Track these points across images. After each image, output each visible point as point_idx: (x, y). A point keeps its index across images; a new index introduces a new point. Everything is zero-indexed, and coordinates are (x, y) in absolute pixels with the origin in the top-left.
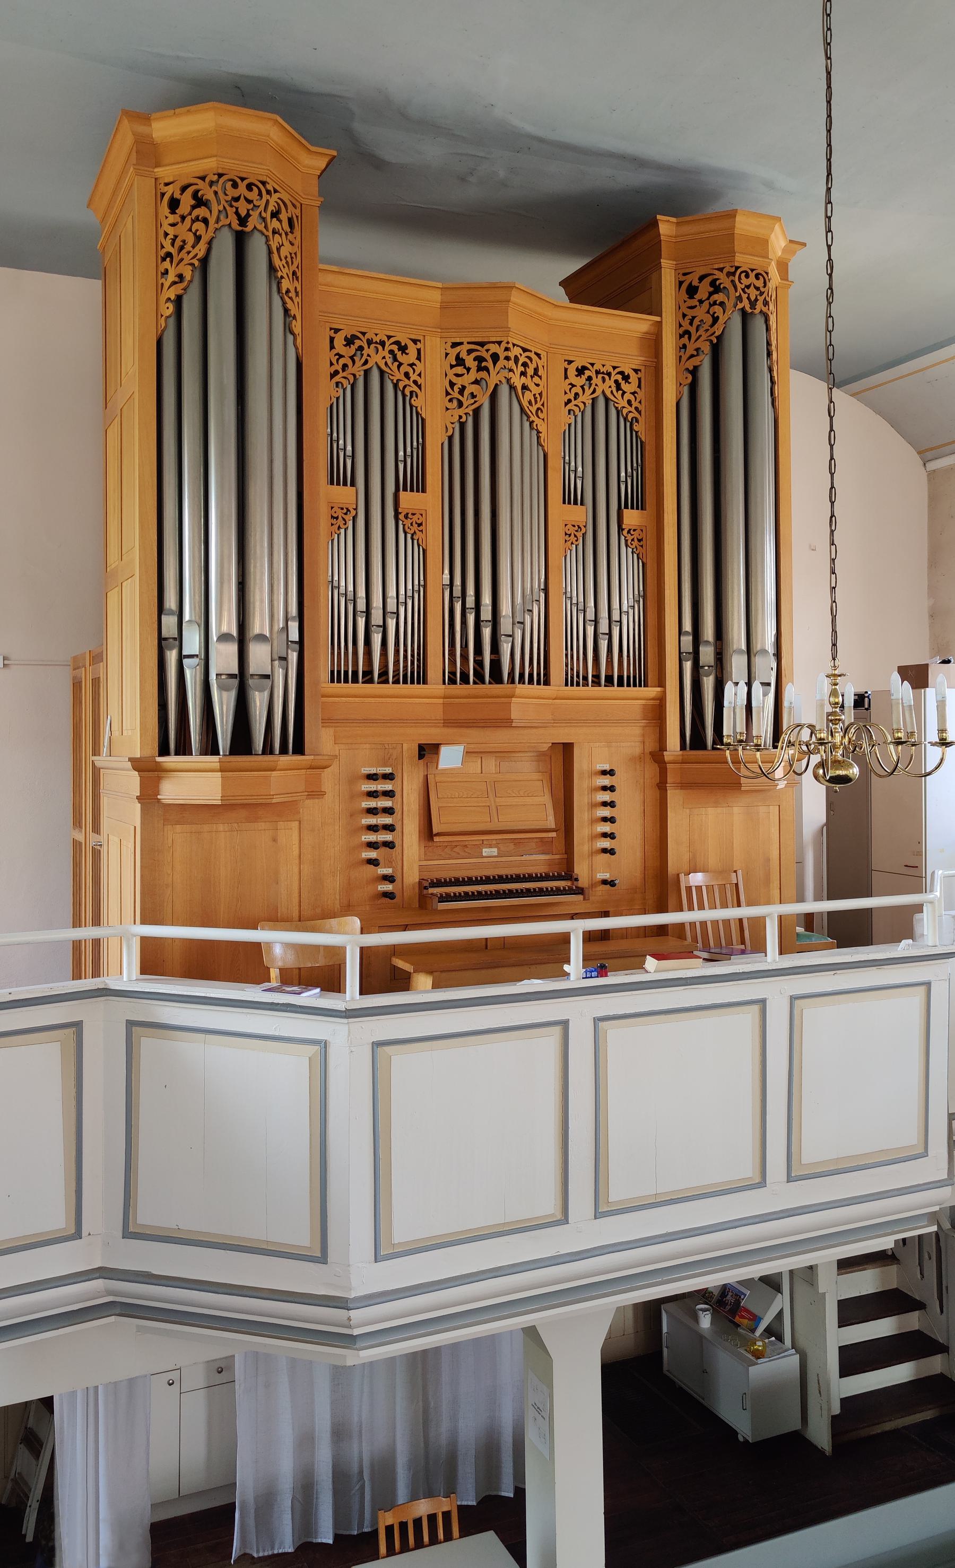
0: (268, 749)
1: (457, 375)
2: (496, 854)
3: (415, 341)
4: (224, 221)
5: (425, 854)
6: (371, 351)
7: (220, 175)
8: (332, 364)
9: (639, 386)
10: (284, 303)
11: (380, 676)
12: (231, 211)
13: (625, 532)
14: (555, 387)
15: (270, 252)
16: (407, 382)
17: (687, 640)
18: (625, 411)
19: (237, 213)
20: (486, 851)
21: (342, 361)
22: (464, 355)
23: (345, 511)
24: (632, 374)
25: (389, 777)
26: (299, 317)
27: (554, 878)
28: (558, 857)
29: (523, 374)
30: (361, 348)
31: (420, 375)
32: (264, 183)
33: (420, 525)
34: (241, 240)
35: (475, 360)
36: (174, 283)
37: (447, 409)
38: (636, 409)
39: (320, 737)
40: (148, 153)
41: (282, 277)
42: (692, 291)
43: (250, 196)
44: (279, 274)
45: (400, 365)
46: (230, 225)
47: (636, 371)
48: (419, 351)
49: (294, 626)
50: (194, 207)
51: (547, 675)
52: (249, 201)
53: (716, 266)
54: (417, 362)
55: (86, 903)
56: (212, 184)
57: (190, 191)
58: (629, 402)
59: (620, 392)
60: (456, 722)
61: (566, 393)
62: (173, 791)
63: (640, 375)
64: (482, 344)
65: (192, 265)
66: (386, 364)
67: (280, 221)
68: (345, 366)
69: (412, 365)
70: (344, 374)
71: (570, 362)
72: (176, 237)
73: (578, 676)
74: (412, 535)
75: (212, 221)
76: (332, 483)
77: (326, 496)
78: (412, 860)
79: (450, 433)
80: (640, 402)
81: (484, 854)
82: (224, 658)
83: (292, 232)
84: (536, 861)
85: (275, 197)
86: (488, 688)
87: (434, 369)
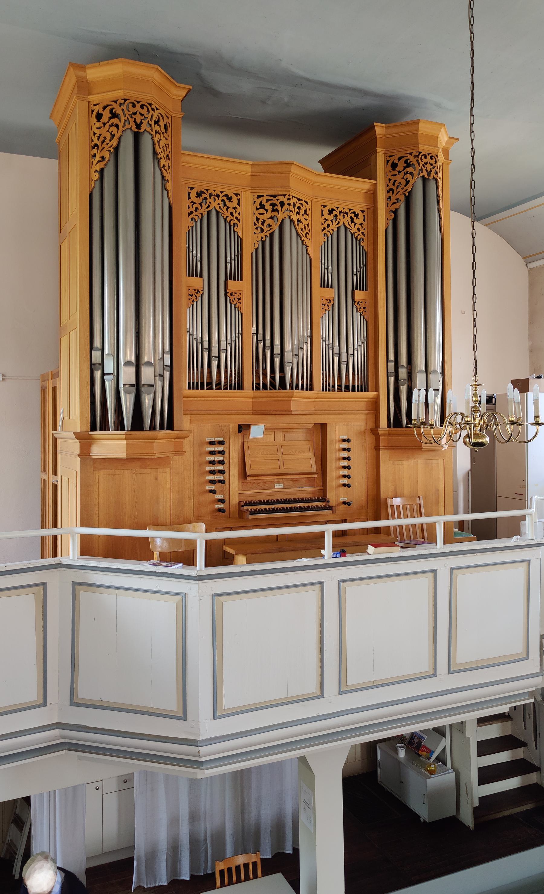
0: (153, 427)
1: (260, 214)
2: (282, 487)
3: (236, 195)
4: (127, 126)
5: (242, 487)
6: (212, 200)
7: (125, 100)
8: (189, 208)
9: (364, 220)
10: (162, 173)
11: (216, 385)
12: (132, 120)
13: (356, 303)
14: (316, 221)
15: (154, 144)
16: (232, 218)
17: (392, 365)
18: (356, 235)
19: (135, 121)
20: (277, 485)
21: (195, 206)
22: (264, 202)
23: (197, 291)
24: (360, 213)
25: (221, 443)
26: (170, 181)
27: (315, 501)
28: (318, 488)
29: (298, 213)
30: (205, 199)
31: (239, 214)
32: (150, 104)
33: (239, 299)
34: (137, 137)
35: (270, 205)
36: (99, 161)
37: (255, 233)
38: (363, 233)
39: (182, 420)
40: (84, 87)
41: (161, 158)
42: (394, 166)
43: (142, 111)
44: (159, 156)
45: (228, 208)
46: (131, 128)
47: (362, 211)
48: (239, 200)
49: (167, 357)
50: (110, 118)
51: (311, 384)
52: (142, 115)
53: (408, 152)
54: (237, 206)
55: (49, 515)
56: (120, 105)
57: (108, 109)
58: (358, 229)
59: (353, 224)
60: (260, 411)
61: (322, 224)
62: (98, 451)
63: (364, 214)
64: (275, 196)
65: (110, 151)
66: (220, 207)
67: (160, 126)
68: (196, 209)
69: (234, 208)
70: (196, 213)
71: (325, 206)
72: (100, 135)
73: (329, 386)
74: (235, 305)
75: (121, 126)
76: (189, 276)
77: (186, 283)
78: (235, 491)
79: (256, 247)
80: (365, 229)
81: (276, 487)
82: (128, 375)
83: (166, 132)
84: (305, 491)
85: (157, 112)
86: (278, 392)
87: (247, 211)
